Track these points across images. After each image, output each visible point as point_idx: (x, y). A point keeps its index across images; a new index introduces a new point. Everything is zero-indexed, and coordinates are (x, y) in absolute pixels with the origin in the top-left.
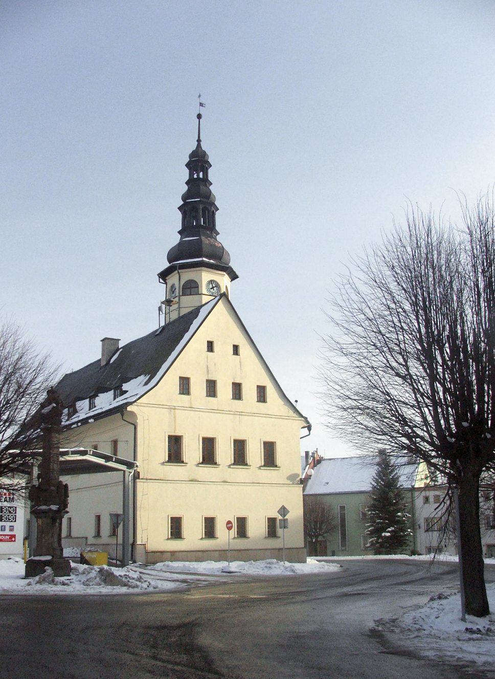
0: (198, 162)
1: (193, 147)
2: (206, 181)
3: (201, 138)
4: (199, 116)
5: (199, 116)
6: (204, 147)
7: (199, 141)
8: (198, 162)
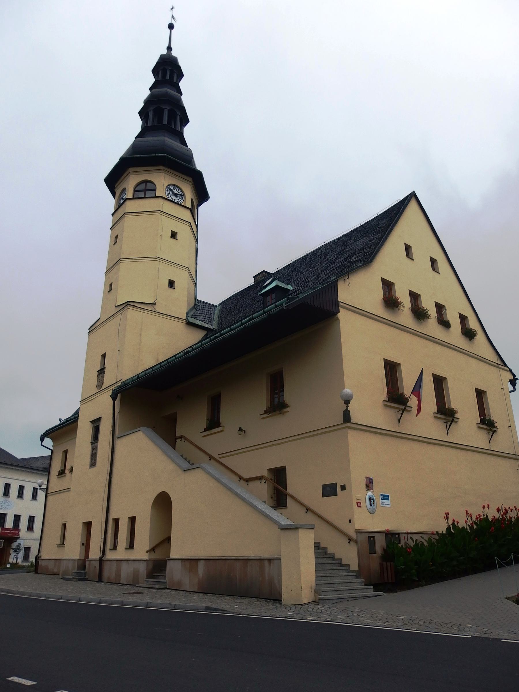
3: (172, 46)
4: (171, 27)
5: (171, 27)
6: (169, 30)
7: (169, 49)
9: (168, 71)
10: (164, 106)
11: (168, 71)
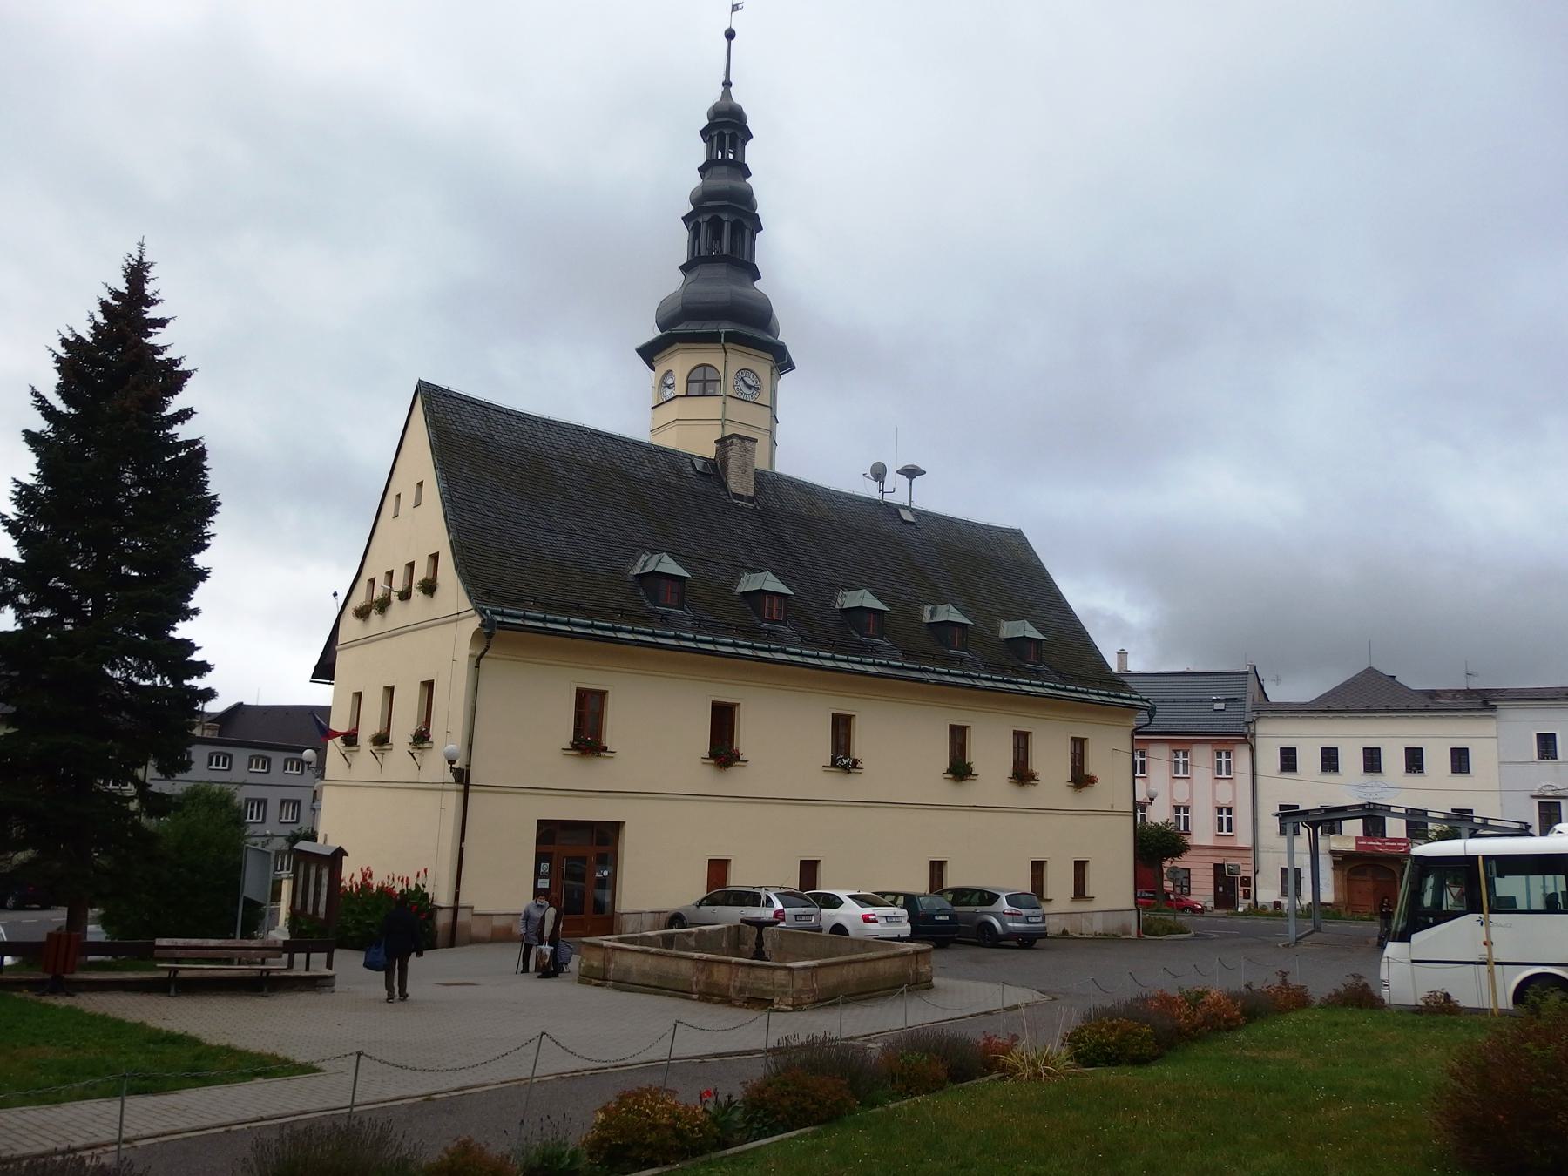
1: (714, 95)
4: (730, 35)
5: (730, 35)
6: (739, 97)
7: (727, 84)
9: (727, 129)
10: (723, 220)
11: (727, 129)
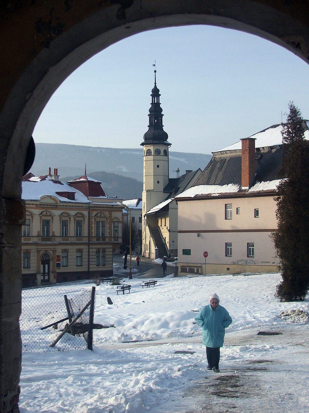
0: (156, 93)
1: (153, 87)
2: (158, 104)
4: (155, 71)
5: (155, 71)
7: (155, 83)
8: (156, 93)
